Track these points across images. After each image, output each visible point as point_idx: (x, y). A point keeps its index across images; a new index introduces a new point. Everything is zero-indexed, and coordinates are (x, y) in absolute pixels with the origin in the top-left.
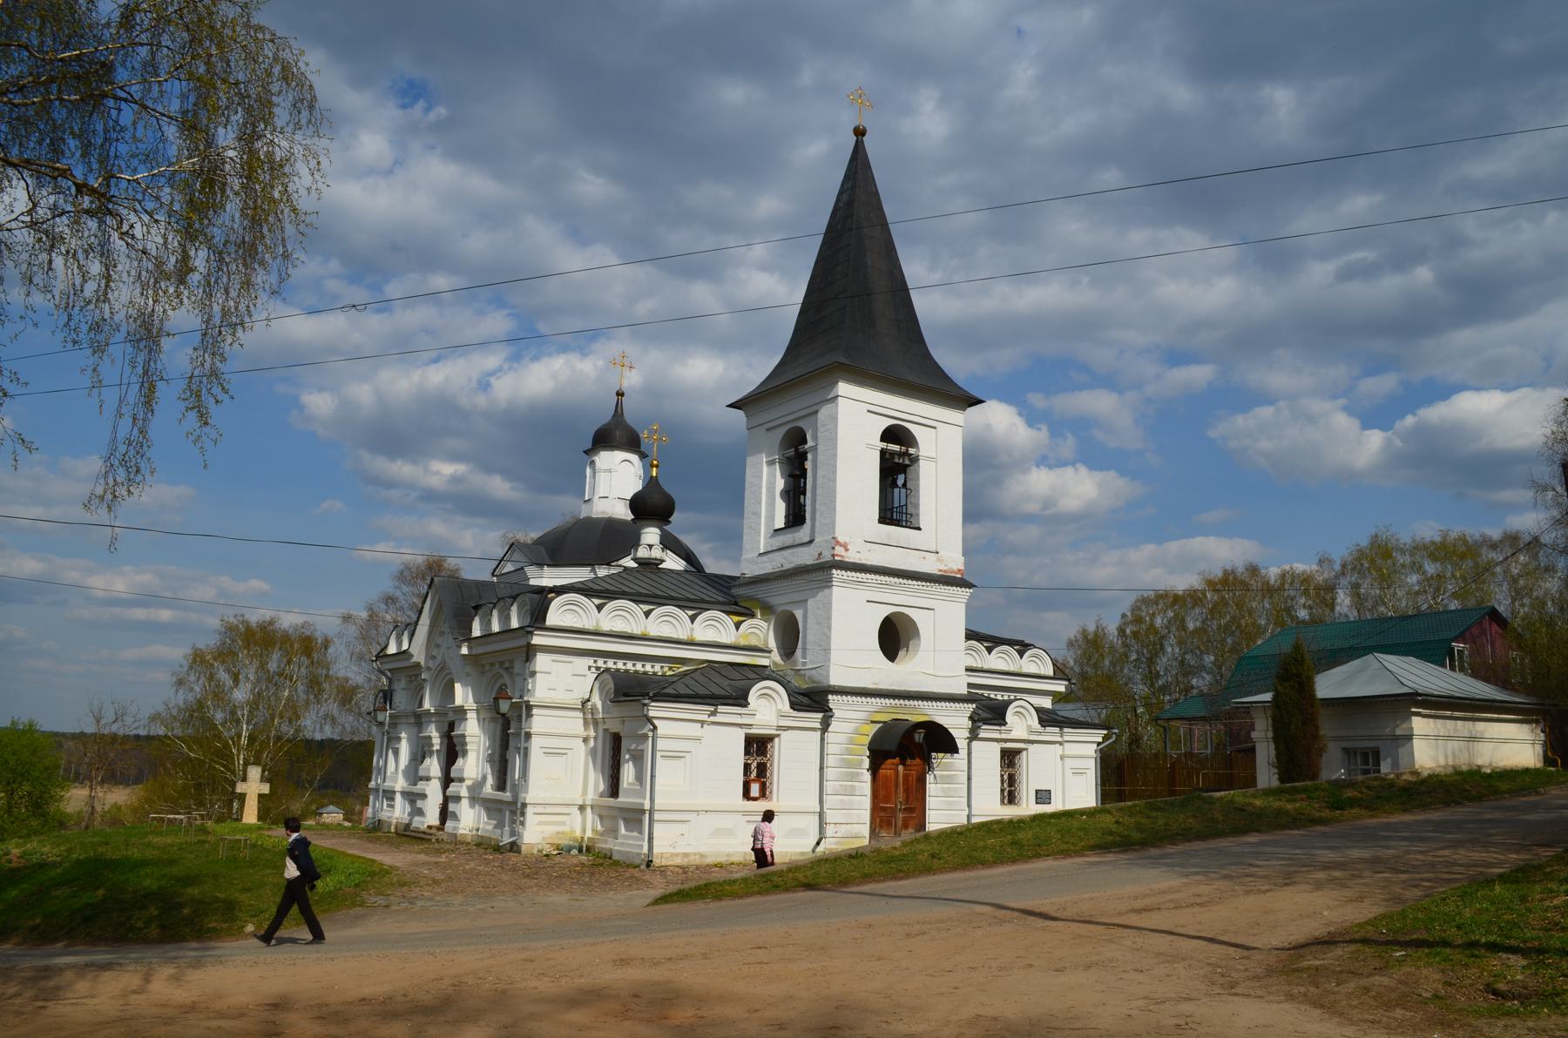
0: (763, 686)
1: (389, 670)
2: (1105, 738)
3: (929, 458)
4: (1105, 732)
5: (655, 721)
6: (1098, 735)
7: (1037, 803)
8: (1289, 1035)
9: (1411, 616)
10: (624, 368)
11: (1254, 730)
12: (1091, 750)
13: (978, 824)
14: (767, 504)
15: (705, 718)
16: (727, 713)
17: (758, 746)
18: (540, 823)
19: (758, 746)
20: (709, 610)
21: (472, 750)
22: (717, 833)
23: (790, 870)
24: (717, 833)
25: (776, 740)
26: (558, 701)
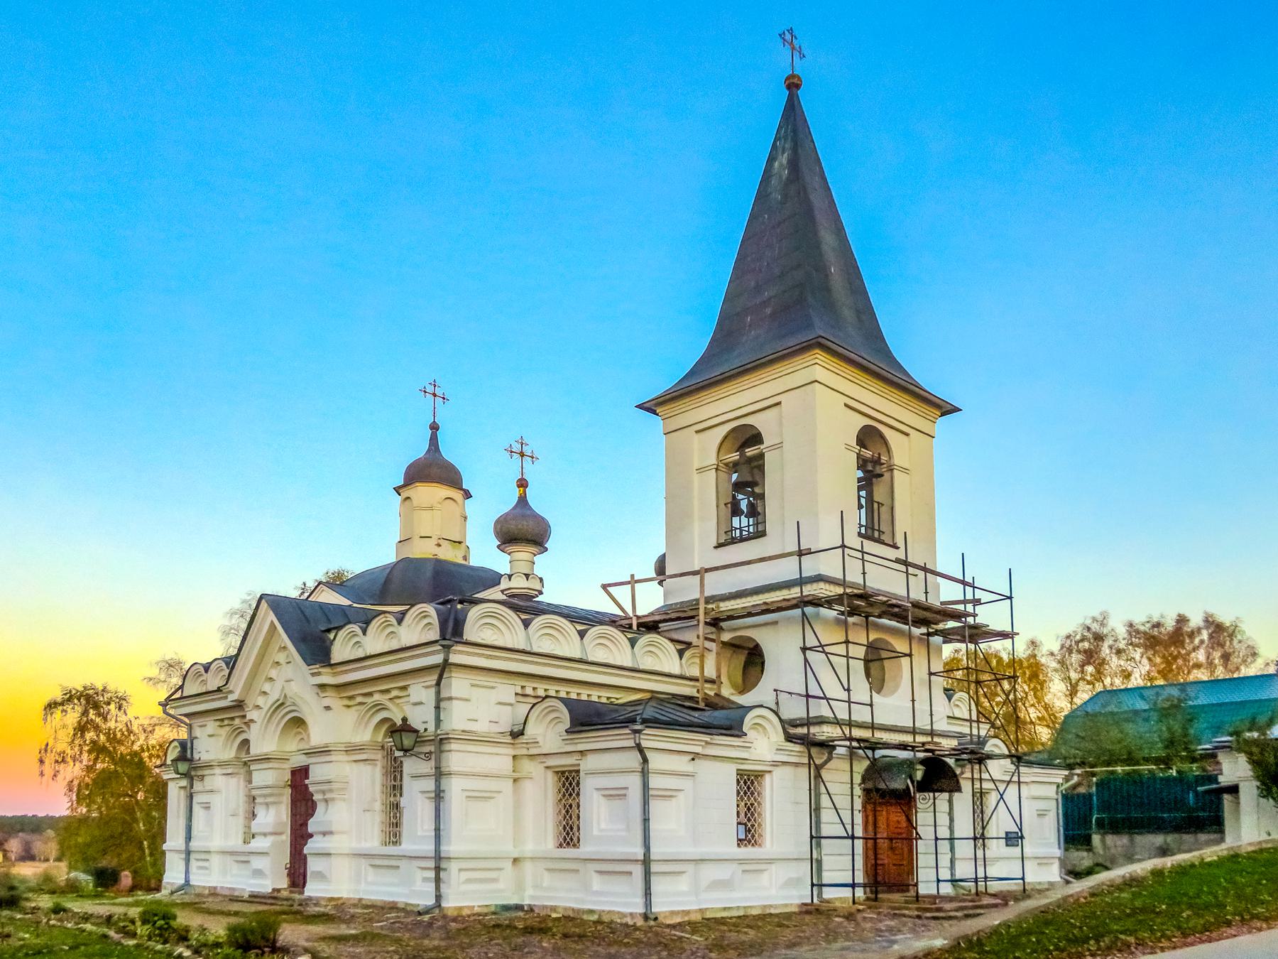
0: (758, 714)
1: (186, 715)
2: (1067, 779)
3: (905, 470)
4: (1066, 773)
5: (649, 755)
6: (1058, 775)
7: (1007, 845)
8: (27, 954)
9: (1252, 677)
10: (436, 398)
11: (1221, 774)
12: (1051, 791)
13: (866, 872)
14: (251, 670)
15: (698, 749)
16: (723, 745)
17: (748, 783)
18: (469, 881)
19: (748, 783)
20: (781, 601)
21: (320, 800)
22: (718, 885)
23: (567, 918)
24: (718, 885)
25: (767, 776)
26: (484, 735)
